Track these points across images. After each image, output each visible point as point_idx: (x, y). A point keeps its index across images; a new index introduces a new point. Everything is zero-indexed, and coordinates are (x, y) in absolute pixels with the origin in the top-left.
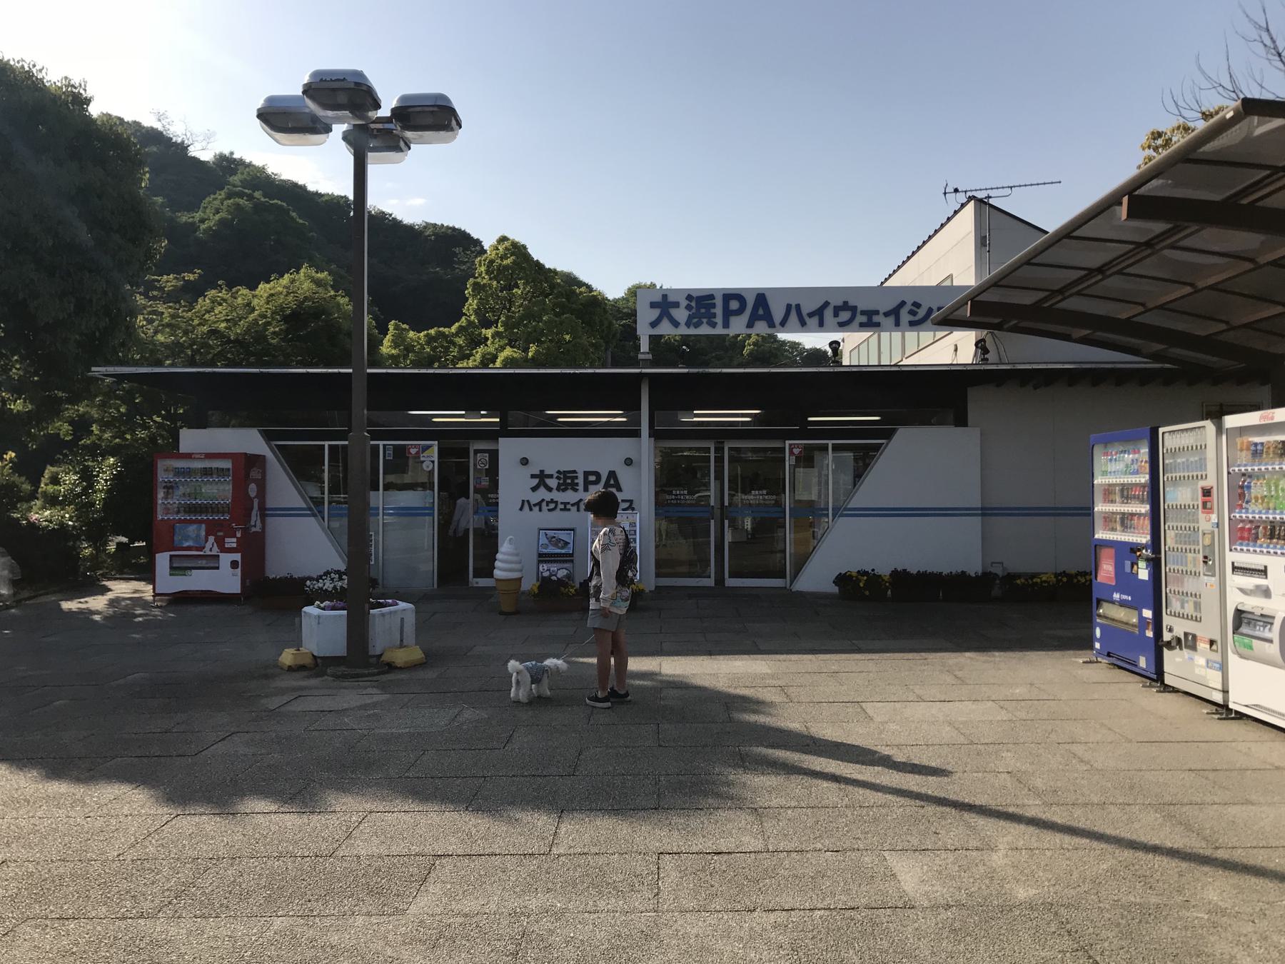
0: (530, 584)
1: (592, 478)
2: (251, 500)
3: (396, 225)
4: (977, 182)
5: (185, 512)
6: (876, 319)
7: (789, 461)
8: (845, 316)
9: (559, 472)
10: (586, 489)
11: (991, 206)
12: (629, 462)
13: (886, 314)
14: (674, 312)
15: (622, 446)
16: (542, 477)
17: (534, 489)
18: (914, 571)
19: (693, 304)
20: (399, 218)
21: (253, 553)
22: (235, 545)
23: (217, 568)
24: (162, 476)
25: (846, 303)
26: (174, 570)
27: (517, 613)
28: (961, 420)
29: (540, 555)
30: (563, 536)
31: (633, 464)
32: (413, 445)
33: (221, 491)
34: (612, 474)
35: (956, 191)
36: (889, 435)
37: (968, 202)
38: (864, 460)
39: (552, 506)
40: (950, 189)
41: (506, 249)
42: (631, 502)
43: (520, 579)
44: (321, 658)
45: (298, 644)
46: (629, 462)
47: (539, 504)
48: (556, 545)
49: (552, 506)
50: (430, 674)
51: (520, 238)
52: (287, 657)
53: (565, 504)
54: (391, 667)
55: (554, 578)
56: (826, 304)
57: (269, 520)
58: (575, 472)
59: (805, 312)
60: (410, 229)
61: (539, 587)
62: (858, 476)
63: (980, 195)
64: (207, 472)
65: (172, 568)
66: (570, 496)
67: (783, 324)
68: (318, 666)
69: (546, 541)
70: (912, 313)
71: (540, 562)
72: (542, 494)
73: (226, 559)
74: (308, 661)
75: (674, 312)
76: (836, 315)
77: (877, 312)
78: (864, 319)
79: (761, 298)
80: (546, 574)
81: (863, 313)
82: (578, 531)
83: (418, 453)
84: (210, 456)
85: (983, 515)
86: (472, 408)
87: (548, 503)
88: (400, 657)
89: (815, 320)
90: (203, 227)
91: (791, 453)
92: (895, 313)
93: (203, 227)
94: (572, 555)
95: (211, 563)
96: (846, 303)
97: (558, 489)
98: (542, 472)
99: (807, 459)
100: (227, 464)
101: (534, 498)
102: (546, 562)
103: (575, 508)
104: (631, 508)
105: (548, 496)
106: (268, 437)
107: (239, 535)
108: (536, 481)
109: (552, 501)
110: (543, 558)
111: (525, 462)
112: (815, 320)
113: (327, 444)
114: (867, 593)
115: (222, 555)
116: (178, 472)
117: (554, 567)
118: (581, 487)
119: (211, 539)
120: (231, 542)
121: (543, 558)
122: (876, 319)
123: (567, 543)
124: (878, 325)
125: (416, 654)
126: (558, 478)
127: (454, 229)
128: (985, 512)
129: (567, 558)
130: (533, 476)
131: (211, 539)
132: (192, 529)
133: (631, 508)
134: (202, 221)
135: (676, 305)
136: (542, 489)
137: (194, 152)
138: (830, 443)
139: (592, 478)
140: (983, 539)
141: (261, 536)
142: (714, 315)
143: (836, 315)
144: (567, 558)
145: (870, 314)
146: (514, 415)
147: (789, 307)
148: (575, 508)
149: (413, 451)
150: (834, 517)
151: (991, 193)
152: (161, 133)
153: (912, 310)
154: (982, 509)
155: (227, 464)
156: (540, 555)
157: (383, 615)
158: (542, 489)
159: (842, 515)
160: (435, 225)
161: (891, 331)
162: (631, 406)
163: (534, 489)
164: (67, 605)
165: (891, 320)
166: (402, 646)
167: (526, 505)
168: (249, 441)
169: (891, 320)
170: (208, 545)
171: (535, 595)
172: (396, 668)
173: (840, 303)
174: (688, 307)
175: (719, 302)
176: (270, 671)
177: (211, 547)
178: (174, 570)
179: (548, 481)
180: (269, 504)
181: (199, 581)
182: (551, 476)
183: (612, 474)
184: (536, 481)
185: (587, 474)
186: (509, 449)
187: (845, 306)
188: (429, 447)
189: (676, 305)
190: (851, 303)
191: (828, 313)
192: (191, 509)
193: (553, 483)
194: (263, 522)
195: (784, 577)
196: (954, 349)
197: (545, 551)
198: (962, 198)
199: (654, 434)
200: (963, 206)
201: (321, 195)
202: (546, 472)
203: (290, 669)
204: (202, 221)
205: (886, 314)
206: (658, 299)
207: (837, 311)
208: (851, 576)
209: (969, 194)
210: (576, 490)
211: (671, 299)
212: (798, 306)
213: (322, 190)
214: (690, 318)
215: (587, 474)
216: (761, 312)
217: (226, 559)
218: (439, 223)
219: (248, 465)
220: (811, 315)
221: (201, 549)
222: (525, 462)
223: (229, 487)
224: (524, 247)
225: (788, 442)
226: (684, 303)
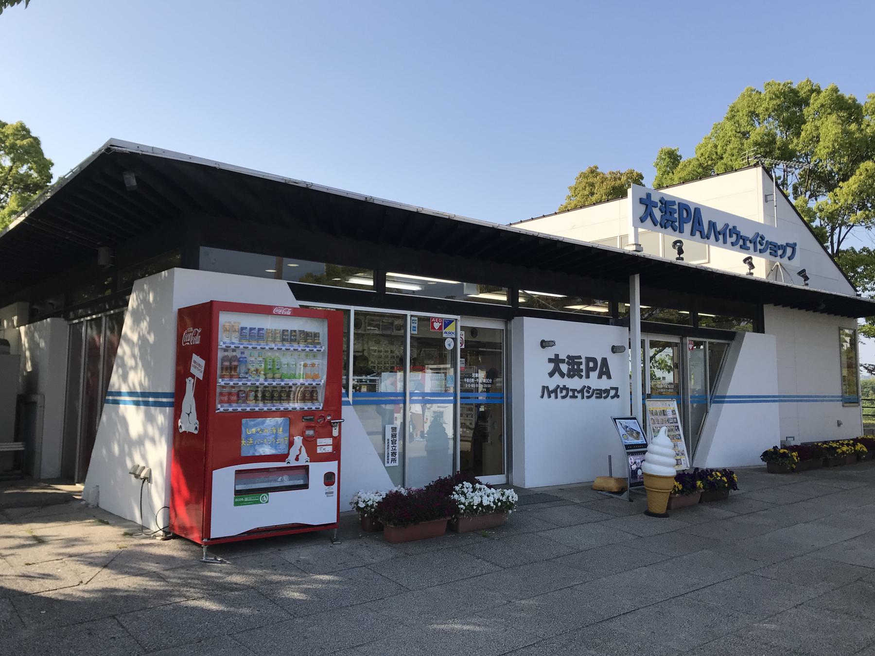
9: (568, 357)
12: (614, 349)
15: (611, 334)
16: (556, 361)
17: (551, 374)
22: (329, 449)
23: (305, 486)
42: (616, 389)
46: (614, 349)
58: (580, 357)
66: (575, 383)
80: (634, 467)
83: (440, 328)
98: (557, 356)
102: (633, 454)
103: (579, 395)
104: (616, 396)
111: (544, 344)
113: (353, 309)
115: (313, 466)
126: (568, 363)
130: (550, 360)
131: (298, 440)
133: (616, 396)
140: (111, 514)
149: (437, 325)
156: (628, 447)
162: (617, 296)
163: (551, 374)
170: (294, 452)
183: (604, 360)
185: (589, 359)
186: (534, 329)
188: (450, 322)
193: (564, 368)
199: (646, 328)
222: (544, 344)
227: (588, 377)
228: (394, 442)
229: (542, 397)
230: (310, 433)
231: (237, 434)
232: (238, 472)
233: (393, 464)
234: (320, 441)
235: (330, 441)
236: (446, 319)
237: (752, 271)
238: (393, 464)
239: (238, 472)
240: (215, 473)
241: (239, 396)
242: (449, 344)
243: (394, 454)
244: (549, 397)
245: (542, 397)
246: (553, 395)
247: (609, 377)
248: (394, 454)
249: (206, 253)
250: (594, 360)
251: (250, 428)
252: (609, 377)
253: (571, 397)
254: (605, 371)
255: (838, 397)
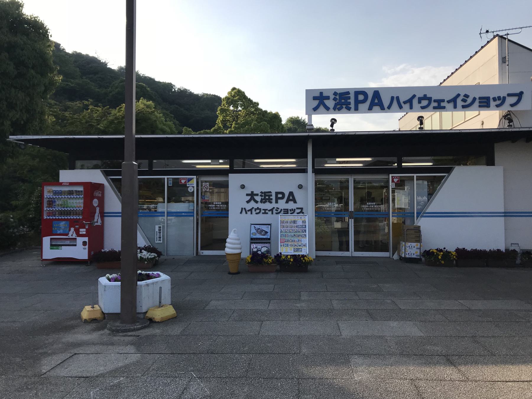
0: (246, 255)
1: (280, 196)
2: (95, 208)
3: (191, 95)
4: (499, 26)
5: (59, 214)
6: (442, 104)
7: (391, 185)
8: (425, 103)
9: (261, 192)
10: (277, 202)
11: (509, 40)
12: (300, 187)
13: (449, 102)
14: (326, 102)
15: (298, 178)
16: (252, 195)
17: (248, 202)
18: (469, 249)
19: (338, 97)
20: (192, 92)
21: (96, 237)
22: (85, 233)
23: (75, 245)
24: (46, 195)
25: (425, 95)
26: (52, 246)
27: (238, 273)
28: (491, 162)
29: (252, 239)
30: (264, 228)
31: (302, 186)
32: (183, 178)
33: (77, 203)
34: (291, 194)
35: (487, 32)
36: (449, 171)
37: (494, 37)
38: (434, 186)
39: (258, 211)
40: (484, 31)
41: (235, 93)
42: (302, 209)
43: (240, 254)
44: (107, 314)
45: (94, 302)
46: (300, 187)
47: (251, 210)
48: (260, 233)
49: (258, 211)
50: (176, 330)
51: (242, 89)
52: (86, 313)
53: (265, 210)
54: (151, 321)
55: (259, 253)
56: (414, 96)
57: (106, 219)
58: (270, 192)
59: (401, 101)
60: (197, 96)
61: (251, 258)
62: (431, 194)
63: (501, 34)
64: (70, 193)
65: (51, 245)
66: (268, 206)
67: (389, 107)
68: (103, 321)
69: (255, 231)
70: (464, 101)
71: (251, 243)
72: (252, 204)
73: (80, 240)
74: (98, 315)
75: (326, 102)
76: (420, 102)
77: (443, 101)
78: (436, 104)
79: (377, 93)
80: (255, 250)
81: (435, 101)
82: (273, 225)
83: (185, 182)
84: (71, 184)
85: (505, 216)
86: (214, 157)
87: (256, 210)
88: (158, 314)
89: (408, 105)
90: (111, 94)
91: (393, 181)
92: (454, 101)
93: (111, 94)
94: (269, 239)
95: (72, 243)
96: (425, 95)
97: (261, 202)
98: (252, 192)
99: (401, 184)
100: (81, 189)
101: (248, 207)
102: (255, 243)
103: (271, 212)
104: (302, 212)
105: (255, 206)
106: (106, 174)
107: (87, 227)
108: (249, 197)
109: (258, 208)
110: (253, 240)
111: (243, 187)
112: (408, 105)
113: (166, 177)
114: (443, 262)
115: (78, 238)
116: (56, 193)
117: (259, 246)
118: (274, 201)
119: (72, 229)
120: (83, 231)
121: (253, 240)
122: (442, 104)
123: (266, 232)
124: (444, 108)
125: (170, 311)
126: (261, 196)
127: (215, 95)
128: (506, 214)
129: (267, 241)
130: (247, 195)
131: (72, 229)
132: (62, 224)
133: (302, 212)
134: (111, 92)
135: (328, 98)
136: (252, 202)
137: (110, 66)
138: (415, 175)
139: (280, 196)
141: (101, 228)
142: (350, 103)
143: (420, 102)
144: (267, 241)
145: (439, 101)
146: (238, 163)
147: (392, 98)
148: (271, 212)
149: (183, 181)
150: (417, 217)
151: (509, 32)
152: (96, 58)
153: (462, 99)
154: (505, 213)
155: (81, 189)
156: (252, 239)
157: (148, 285)
158: (252, 202)
159: (422, 216)
160: (207, 94)
161: (452, 111)
162: (301, 155)
163: (248, 202)
164: (431, 164)
165: (452, 105)
166: (160, 305)
167: (244, 211)
168: (96, 176)
169: (452, 105)
170: (71, 233)
171: (249, 263)
172: (156, 322)
173: (421, 95)
174: (335, 99)
175: (352, 96)
176: (73, 322)
177: (72, 233)
178: (52, 246)
179: (256, 197)
180: (107, 210)
181: (65, 252)
182: (257, 195)
183: (291, 194)
184: (249, 197)
185: (277, 193)
186: (234, 180)
187: (425, 97)
188: (191, 179)
189: (328, 98)
190: (428, 96)
191: (415, 101)
192: (61, 213)
193: (258, 198)
194: (103, 220)
195: (387, 250)
196: (489, 120)
197: (255, 237)
198: (490, 36)
199: (316, 172)
200: (492, 40)
201: (161, 83)
202: (254, 193)
203: (86, 321)
204: (111, 92)
205: (449, 102)
206: (318, 95)
207: (420, 100)
208: (433, 252)
209: (495, 34)
210: (271, 203)
211: (324, 95)
212: (398, 98)
213: (161, 81)
214: (336, 105)
215: (277, 193)
216: (376, 101)
217: (80, 240)
218: (209, 93)
219: (92, 190)
220: (405, 103)
221: (67, 235)
222: (243, 187)
223: (82, 201)
224: (244, 93)
225: (391, 175)
226: (332, 97)
227: (277, 202)
228: (160, 233)
229: (241, 213)
230: (77, 227)
231: (52, 226)
232: (51, 239)
233: (159, 242)
234: (81, 230)
235: (85, 230)
236: (188, 178)
237: (422, 126)
238: (159, 242)
239: (51, 239)
240: (44, 238)
241: (53, 213)
242: (190, 190)
243: (160, 238)
244: (246, 213)
245: (241, 213)
246: (250, 212)
247: (295, 202)
248: (160, 238)
249: (79, 163)
250: (283, 194)
251: (55, 224)
252: (295, 202)
253: (263, 213)
254: (291, 198)
255: (142, 216)
